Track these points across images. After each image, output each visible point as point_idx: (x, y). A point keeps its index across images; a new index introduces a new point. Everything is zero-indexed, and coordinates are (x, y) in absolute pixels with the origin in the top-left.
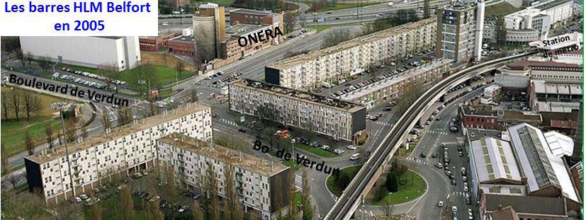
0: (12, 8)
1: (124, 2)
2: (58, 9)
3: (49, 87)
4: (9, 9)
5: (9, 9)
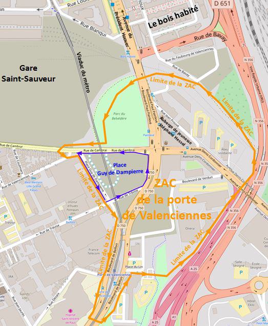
0: (153, 25)
1: (183, 203)
2: (34, 69)
3: (147, 216)
4: (151, 25)
5: (151, 25)
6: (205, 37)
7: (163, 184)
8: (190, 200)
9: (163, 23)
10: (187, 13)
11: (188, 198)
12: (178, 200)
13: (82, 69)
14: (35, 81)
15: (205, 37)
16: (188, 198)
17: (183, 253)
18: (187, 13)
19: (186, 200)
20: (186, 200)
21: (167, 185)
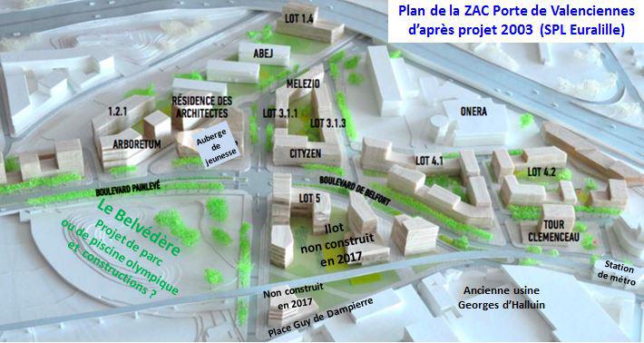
0: (107, 208)
2: (442, 31)
3: (559, 11)
6: (428, 12)
7: (475, 12)
8: (519, 12)
9: (340, 230)
10: (163, 284)
11: (517, 9)
12: (505, 12)
13: (428, 12)
14: (609, 9)
15: (529, 13)
16: (517, 9)
17: (524, 12)
18: (163, 284)
19: (514, 12)
20: (514, 12)
21: (478, 12)
